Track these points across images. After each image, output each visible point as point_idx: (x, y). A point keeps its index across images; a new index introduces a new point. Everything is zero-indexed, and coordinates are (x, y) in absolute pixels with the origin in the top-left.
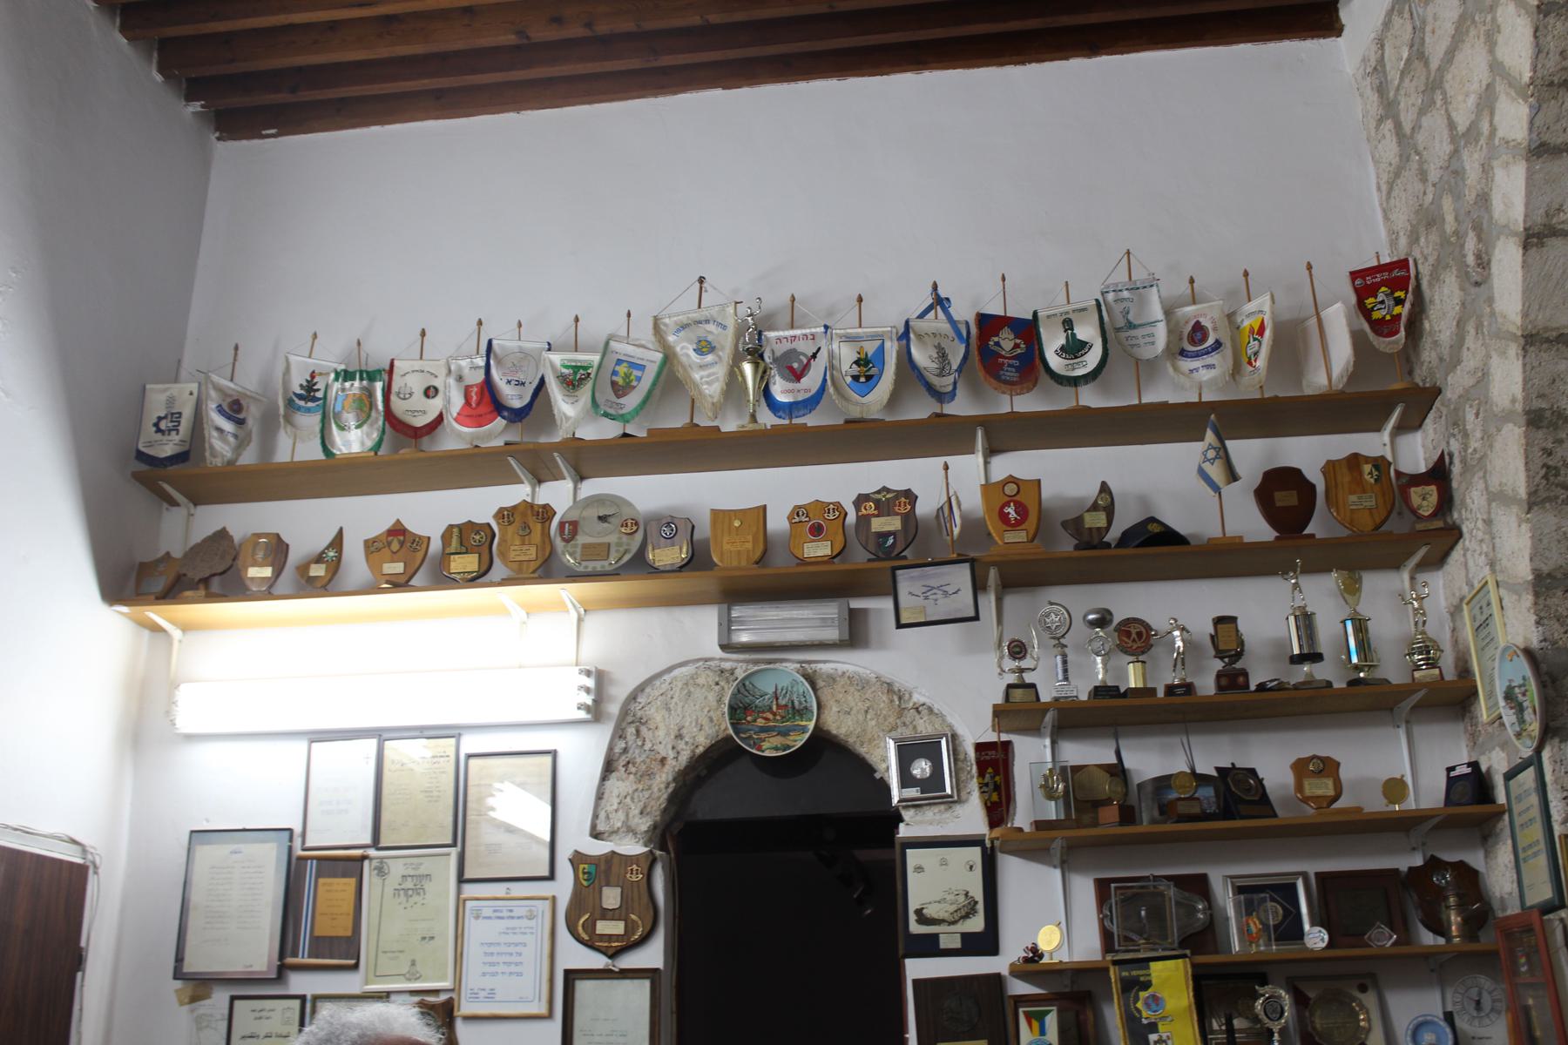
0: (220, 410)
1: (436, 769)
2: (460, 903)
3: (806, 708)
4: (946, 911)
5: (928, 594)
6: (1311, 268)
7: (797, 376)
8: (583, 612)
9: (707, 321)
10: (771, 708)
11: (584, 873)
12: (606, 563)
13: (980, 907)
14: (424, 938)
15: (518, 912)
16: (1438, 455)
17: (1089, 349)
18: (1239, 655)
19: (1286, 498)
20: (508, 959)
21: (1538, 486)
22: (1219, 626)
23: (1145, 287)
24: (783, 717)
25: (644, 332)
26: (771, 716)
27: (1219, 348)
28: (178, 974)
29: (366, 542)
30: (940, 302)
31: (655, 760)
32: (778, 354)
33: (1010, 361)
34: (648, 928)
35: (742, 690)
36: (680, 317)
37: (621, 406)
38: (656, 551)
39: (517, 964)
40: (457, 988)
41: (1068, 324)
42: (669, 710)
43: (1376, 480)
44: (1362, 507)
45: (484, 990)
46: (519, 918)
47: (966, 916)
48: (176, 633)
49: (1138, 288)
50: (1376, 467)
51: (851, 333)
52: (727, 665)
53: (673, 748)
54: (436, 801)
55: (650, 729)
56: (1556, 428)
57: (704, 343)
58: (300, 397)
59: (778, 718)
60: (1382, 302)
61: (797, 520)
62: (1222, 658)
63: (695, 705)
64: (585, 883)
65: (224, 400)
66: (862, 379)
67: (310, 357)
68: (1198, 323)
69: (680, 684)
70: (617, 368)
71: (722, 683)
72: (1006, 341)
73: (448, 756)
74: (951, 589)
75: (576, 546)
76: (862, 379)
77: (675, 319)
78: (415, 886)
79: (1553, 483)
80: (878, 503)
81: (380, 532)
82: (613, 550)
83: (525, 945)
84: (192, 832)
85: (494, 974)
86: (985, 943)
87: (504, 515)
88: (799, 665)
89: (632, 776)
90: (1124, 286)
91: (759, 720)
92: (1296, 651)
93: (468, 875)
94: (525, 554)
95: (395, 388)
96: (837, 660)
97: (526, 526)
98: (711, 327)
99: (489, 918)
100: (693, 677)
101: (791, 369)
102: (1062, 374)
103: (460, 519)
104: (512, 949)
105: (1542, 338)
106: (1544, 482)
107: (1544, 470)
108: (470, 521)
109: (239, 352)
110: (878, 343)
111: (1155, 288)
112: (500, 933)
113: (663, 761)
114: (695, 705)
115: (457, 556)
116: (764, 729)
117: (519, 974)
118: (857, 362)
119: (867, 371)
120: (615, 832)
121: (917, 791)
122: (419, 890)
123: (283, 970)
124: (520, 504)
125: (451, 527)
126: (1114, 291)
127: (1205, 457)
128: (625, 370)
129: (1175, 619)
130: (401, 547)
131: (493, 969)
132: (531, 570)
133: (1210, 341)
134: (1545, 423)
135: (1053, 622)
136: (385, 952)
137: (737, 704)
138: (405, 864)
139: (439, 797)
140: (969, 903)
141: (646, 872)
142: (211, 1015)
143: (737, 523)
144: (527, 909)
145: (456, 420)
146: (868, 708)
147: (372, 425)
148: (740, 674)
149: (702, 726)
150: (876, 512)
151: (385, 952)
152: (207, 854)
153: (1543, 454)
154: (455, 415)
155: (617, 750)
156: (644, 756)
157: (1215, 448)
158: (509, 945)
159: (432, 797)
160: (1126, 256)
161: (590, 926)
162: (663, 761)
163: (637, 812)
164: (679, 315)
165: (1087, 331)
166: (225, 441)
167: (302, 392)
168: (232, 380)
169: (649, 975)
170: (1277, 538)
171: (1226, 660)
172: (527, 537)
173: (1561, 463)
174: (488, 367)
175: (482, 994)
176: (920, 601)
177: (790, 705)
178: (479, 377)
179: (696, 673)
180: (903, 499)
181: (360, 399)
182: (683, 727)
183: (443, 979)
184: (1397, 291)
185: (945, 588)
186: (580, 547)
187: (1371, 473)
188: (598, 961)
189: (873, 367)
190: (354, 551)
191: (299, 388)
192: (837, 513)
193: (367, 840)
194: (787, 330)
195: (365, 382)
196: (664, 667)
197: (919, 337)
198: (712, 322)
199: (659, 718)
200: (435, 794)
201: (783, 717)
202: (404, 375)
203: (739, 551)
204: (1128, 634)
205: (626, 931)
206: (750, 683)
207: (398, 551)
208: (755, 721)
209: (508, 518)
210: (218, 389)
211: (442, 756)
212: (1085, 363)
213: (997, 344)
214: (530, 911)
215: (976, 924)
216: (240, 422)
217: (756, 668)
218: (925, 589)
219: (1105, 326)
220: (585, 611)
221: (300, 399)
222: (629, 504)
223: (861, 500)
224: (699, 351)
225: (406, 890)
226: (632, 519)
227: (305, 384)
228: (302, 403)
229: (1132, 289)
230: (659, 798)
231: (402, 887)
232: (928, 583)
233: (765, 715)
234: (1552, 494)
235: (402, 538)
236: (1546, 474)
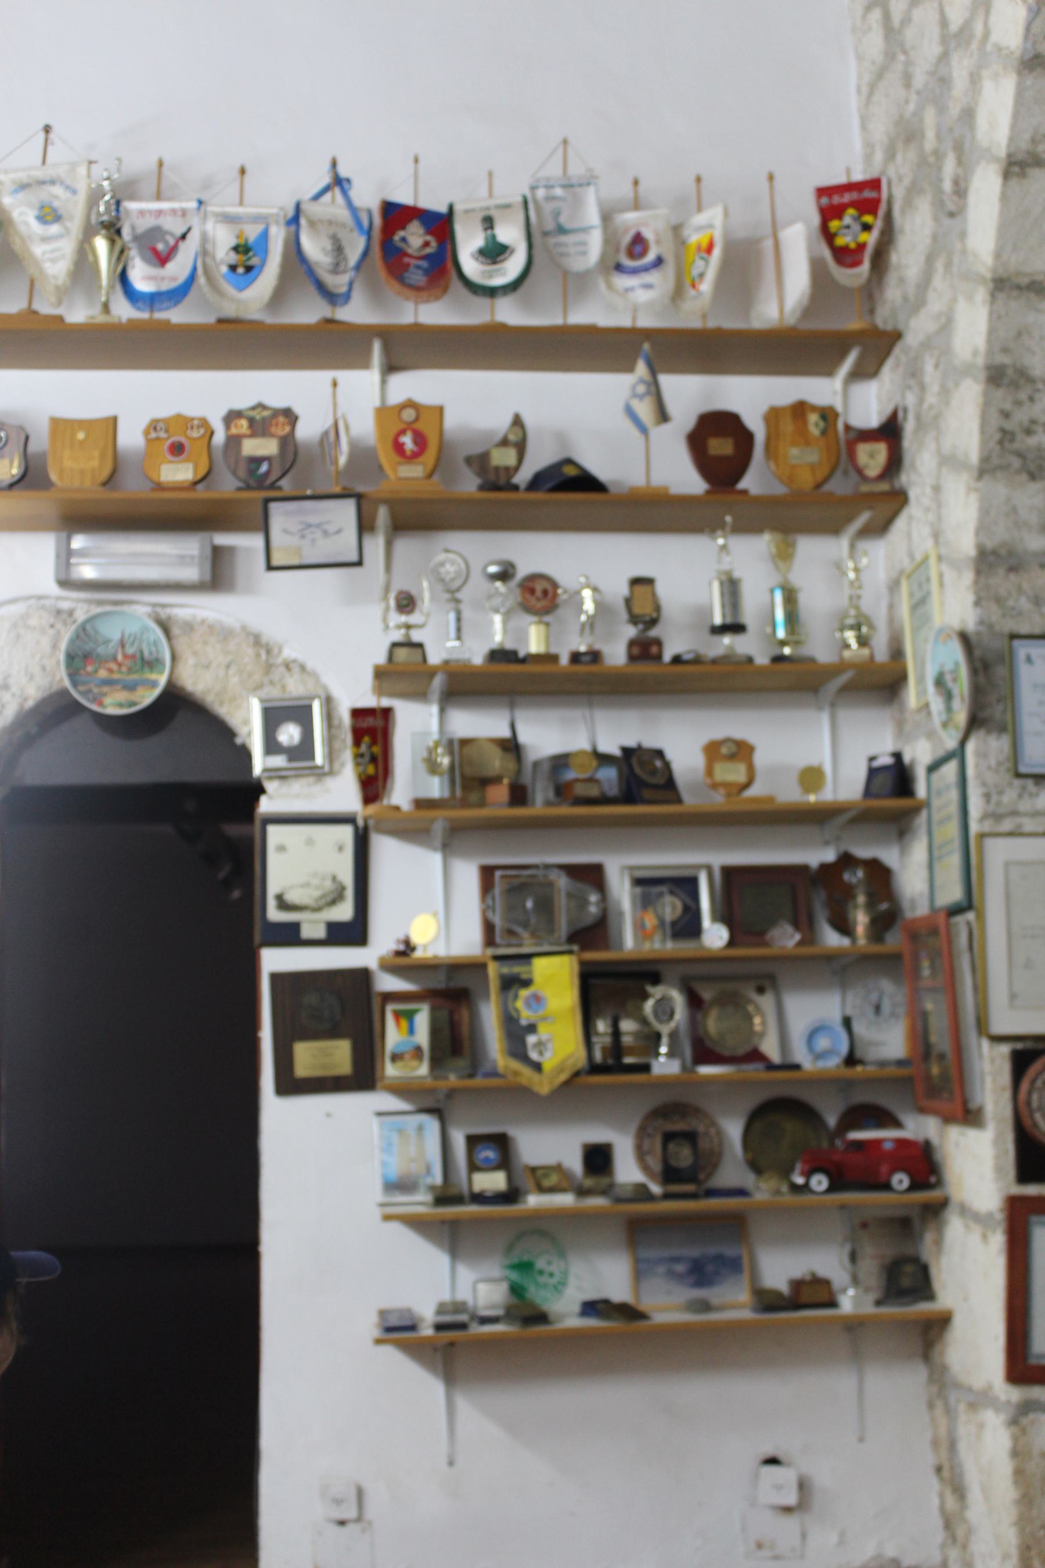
9: (53, 182)
32: (140, 230)
35: (82, 634)
41: (488, 222)
47: (333, 902)
52: (65, 605)
57: (47, 210)
66: (241, 270)
74: (331, 528)
76: (241, 270)
98: (58, 190)
101: (155, 251)
110: (259, 228)
118: (236, 249)
133: (651, 257)
165: (509, 233)
185: (326, 527)
187: (816, 425)
208: (96, 671)
215: (344, 912)
223: (232, 417)
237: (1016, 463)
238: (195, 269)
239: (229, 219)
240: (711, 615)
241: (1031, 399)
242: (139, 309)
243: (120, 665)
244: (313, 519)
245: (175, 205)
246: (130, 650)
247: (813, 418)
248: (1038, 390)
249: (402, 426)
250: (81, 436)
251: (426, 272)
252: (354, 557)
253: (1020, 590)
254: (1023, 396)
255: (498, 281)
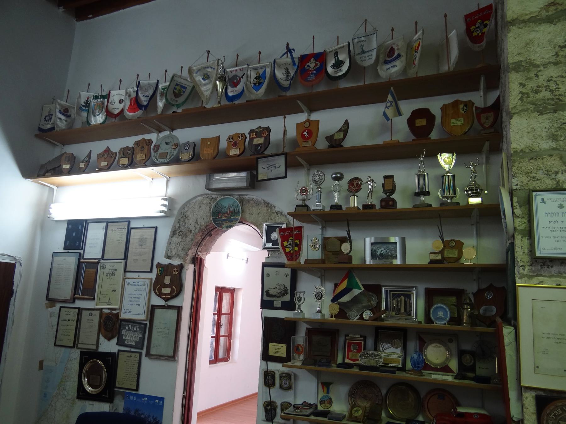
0: (60, 112)
1: (122, 233)
2: (124, 280)
3: (238, 211)
4: (277, 292)
5: (269, 168)
6: (446, 16)
7: (235, 85)
8: (169, 178)
9: (208, 67)
10: (227, 212)
11: (159, 271)
12: (165, 159)
13: (289, 291)
14: (113, 291)
15: (141, 283)
16: (497, 97)
17: (344, 64)
18: (393, 192)
19: (421, 122)
20: (136, 299)
21: (516, 104)
22: (386, 180)
23: (371, 35)
24: (231, 215)
25: (185, 73)
26: (227, 215)
27: (399, 57)
28: (47, 299)
29: (97, 155)
30: (289, 51)
31: (188, 231)
32: (230, 77)
33: (313, 72)
34: (178, 291)
35: (217, 206)
36: (199, 67)
37: (177, 101)
38: (182, 154)
39: (138, 301)
40: (120, 309)
41: (336, 54)
42: (194, 212)
43: (465, 112)
44: (457, 124)
45: (128, 310)
46: (140, 285)
47: (284, 295)
48: (55, 188)
49: (368, 35)
50: (466, 106)
51: (255, 67)
52: (214, 196)
53: (194, 226)
54: (121, 244)
55: (188, 220)
56: (529, 70)
57: (206, 76)
58: (84, 106)
59: (229, 216)
60: (478, 27)
61: (229, 141)
62: (386, 194)
63: (202, 211)
64: (160, 274)
65: (61, 109)
66: (257, 85)
67: (87, 92)
68: (392, 47)
69: (197, 203)
70: (176, 87)
71: (211, 203)
72: (312, 64)
73: (125, 229)
74: (277, 166)
75: (157, 154)
76: (257, 85)
77: (197, 67)
78: (112, 274)
79: (525, 102)
80: (256, 133)
81: (102, 151)
82: (169, 154)
83: (141, 295)
84: (53, 252)
85: (132, 305)
86: (290, 306)
87: (137, 143)
88: (238, 196)
89: (180, 236)
90: (362, 35)
91: (223, 217)
92: (417, 191)
93: (127, 270)
94: (142, 157)
95: (110, 101)
96: (251, 194)
97: (143, 147)
98: (209, 70)
99: (132, 285)
100: (202, 201)
101: (234, 83)
102: (333, 75)
103: (124, 146)
104: (138, 296)
105: (520, 20)
106: (520, 101)
107: (520, 95)
108: (127, 146)
109: (69, 92)
110: (263, 70)
111: (375, 34)
112: (135, 290)
113: (191, 231)
114: (202, 211)
115: (122, 159)
116: (224, 220)
117: (139, 305)
118: (256, 78)
119: (259, 81)
120: (174, 256)
121: (271, 245)
122: (113, 274)
123: (73, 300)
124: (142, 139)
125: (122, 148)
126: (357, 38)
127: (386, 106)
128: (179, 88)
129: (369, 177)
130: (107, 156)
131: (131, 303)
132: (143, 163)
133: (396, 55)
134: (522, 68)
135: (317, 178)
136: (102, 295)
137: (215, 211)
138: (110, 265)
139: (121, 242)
140: (285, 290)
141: (179, 271)
142: (55, 312)
143: (209, 143)
144: (144, 282)
145: (127, 111)
146: (259, 212)
147: (103, 114)
148: (218, 199)
149: (203, 219)
150: (256, 137)
151: (102, 295)
152: (56, 259)
153: (520, 86)
154: (127, 109)
155: (177, 227)
156: (185, 229)
157: (390, 102)
158: (137, 294)
159: (120, 242)
160: (365, 22)
161: (160, 290)
162: (191, 231)
163: (181, 249)
164: (198, 66)
165: (342, 57)
166: (62, 123)
167: (85, 104)
168: (66, 102)
169: (178, 308)
170: (413, 140)
171: (388, 194)
172: (143, 151)
173: (531, 91)
174: (137, 91)
175: (128, 311)
176: (266, 171)
177: (233, 211)
178: (134, 95)
179: (203, 200)
180: (265, 131)
181: (100, 105)
182: (198, 219)
183: (117, 305)
184: (485, 21)
185: (275, 165)
186: (159, 154)
187: (463, 109)
188: (161, 302)
189: (262, 79)
190: (94, 157)
191: (83, 103)
192: (242, 138)
193: (100, 256)
194: (235, 67)
195: (101, 99)
196: (192, 197)
197: (279, 66)
198: (209, 68)
199: (190, 216)
200: (121, 241)
201: (231, 215)
202: (113, 96)
203: (209, 153)
204: (353, 184)
205: (171, 292)
206: (220, 203)
207: (107, 157)
208: (222, 217)
209: (138, 144)
210: (60, 104)
211: (123, 229)
212: (341, 70)
213: (308, 66)
214: (144, 283)
215: (287, 298)
216: (69, 116)
217: (223, 197)
218: (268, 166)
219: (351, 53)
220: (170, 177)
221: (83, 107)
222: (177, 139)
223: (251, 131)
224: (204, 79)
225: (110, 274)
226: (176, 143)
227: (85, 101)
228: (84, 108)
229: (366, 36)
230: (189, 244)
231: (109, 273)
232: (269, 163)
233: (225, 215)
234: (525, 108)
235: (108, 153)
236: (522, 97)
237: (532, 107)
238: (244, 88)
239: (254, 69)
240: (415, 190)
241: (537, 76)
242: (229, 102)
243: (228, 214)
244: (271, 163)
245: (241, 67)
246: (231, 210)
247: (461, 106)
248: (540, 71)
249: (305, 129)
250: (209, 143)
251: (315, 74)
252: (284, 175)
253: (538, 168)
254: (532, 75)
255: (340, 74)
